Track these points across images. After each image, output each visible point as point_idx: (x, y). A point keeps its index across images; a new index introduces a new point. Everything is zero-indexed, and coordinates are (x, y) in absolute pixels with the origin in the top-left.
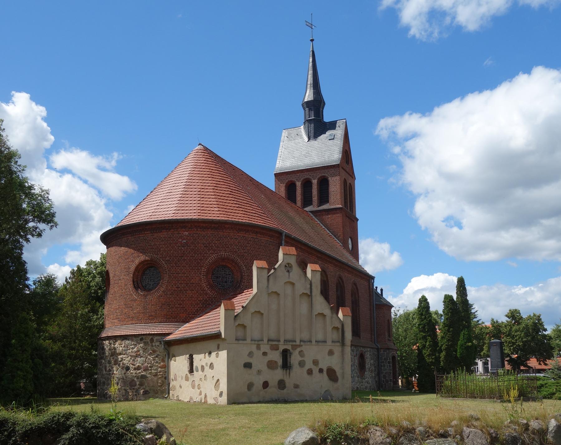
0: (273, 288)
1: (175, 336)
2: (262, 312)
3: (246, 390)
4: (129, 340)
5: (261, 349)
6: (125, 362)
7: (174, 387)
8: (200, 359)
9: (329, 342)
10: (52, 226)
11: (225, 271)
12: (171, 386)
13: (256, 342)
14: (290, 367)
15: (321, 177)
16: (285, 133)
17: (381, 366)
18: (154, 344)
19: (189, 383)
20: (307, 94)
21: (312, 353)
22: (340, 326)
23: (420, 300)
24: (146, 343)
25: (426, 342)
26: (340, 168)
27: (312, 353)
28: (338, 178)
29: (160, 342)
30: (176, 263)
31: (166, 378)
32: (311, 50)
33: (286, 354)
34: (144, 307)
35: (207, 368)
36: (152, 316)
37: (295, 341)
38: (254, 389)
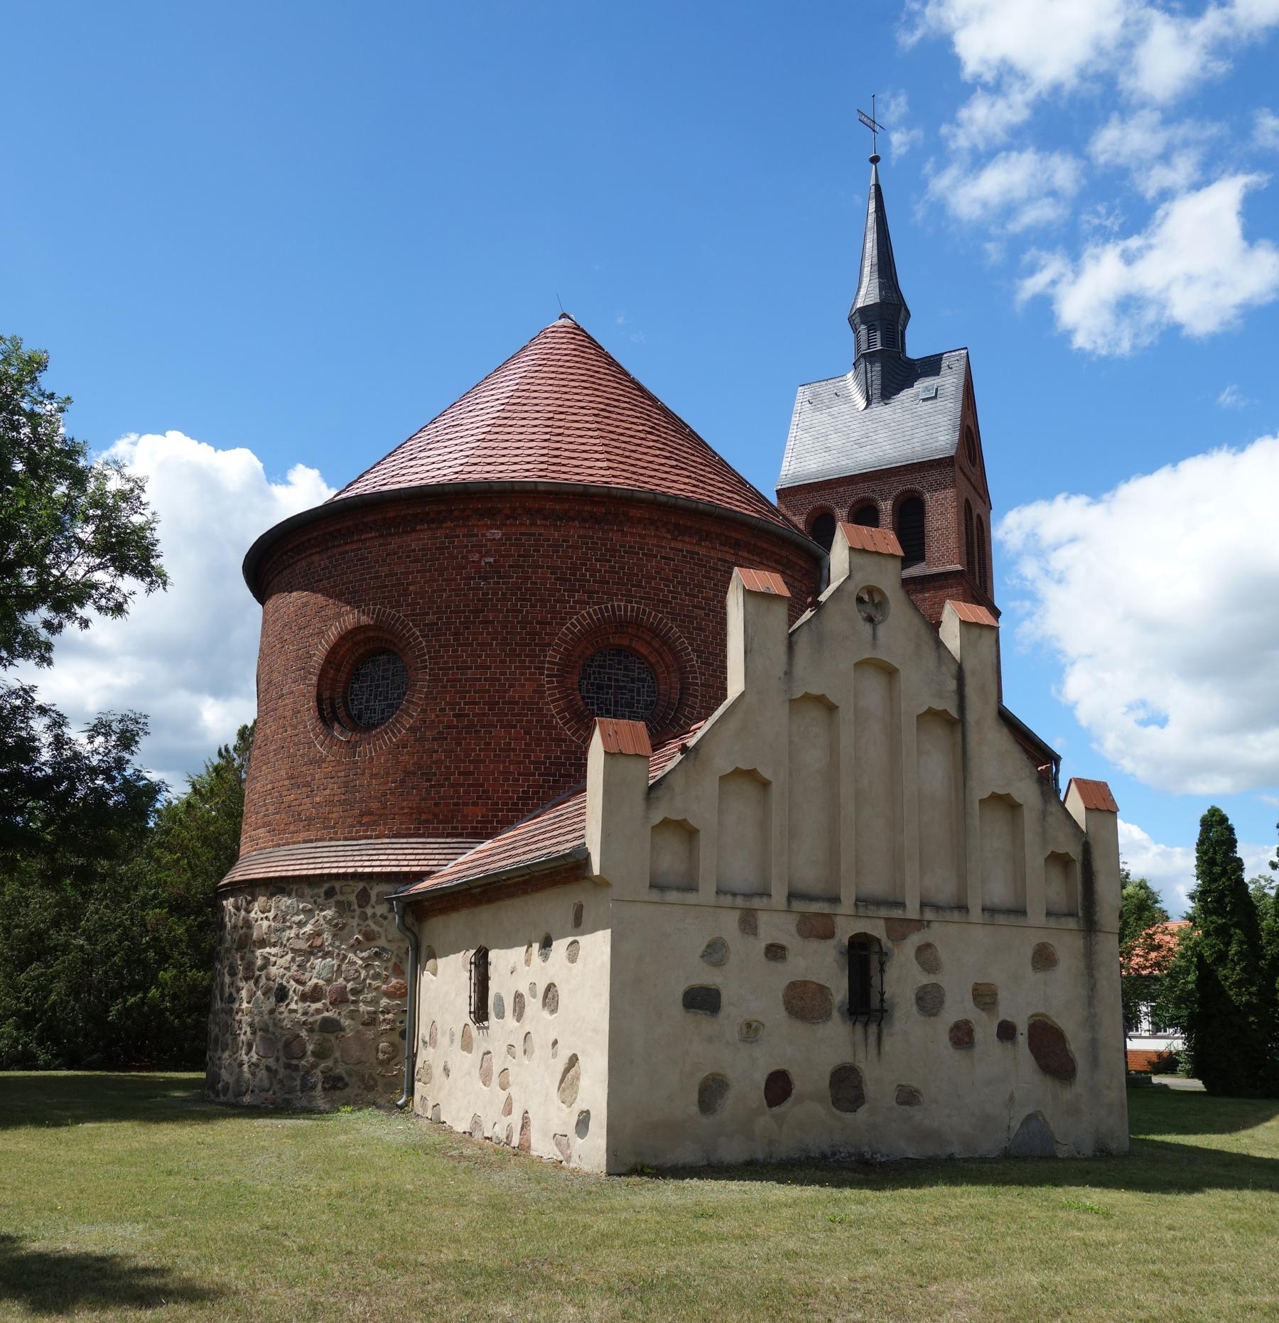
0: (811, 681)
1: (436, 881)
2: (766, 773)
3: (694, 1109)
4: (289, 895)
5: (762, 930)
6: (273, 970)
7: (428, 1067)
8: (513, 968)
9: (1036, 915)
10: (152, 582)
12: (419, 1064)
13: (740, 902)
14: (883, 1011)
15: (903, 493)
16: (802, 394)
18: (369, 911)
19: (473, 1059)
20: (863, 292)
22: (1074, 851)
23: (1204, 822)
24: (343, 908)
25: (1228, 944)
26: (957, 468)
27: (968, 954)
28: (950, 493)
29: (390, 901)
30: (456, 634)
31: (405, 1033)
32: (873, 181)
33: (862, 957)
34: (346, 785)
35: (533, 1005)
36: (371, 813)
37: (901, 905)
38: (729, 1106)
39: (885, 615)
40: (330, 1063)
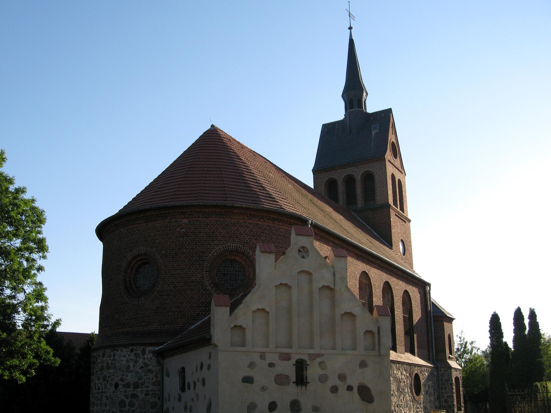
2: (267, 309)
11: (234, 267)
17: (442, 389)
18: (146, 356)
21: (337, 363)
22: (375, 330)
33: (301, 366)
39: (308, 256)
40: (134, 408)
